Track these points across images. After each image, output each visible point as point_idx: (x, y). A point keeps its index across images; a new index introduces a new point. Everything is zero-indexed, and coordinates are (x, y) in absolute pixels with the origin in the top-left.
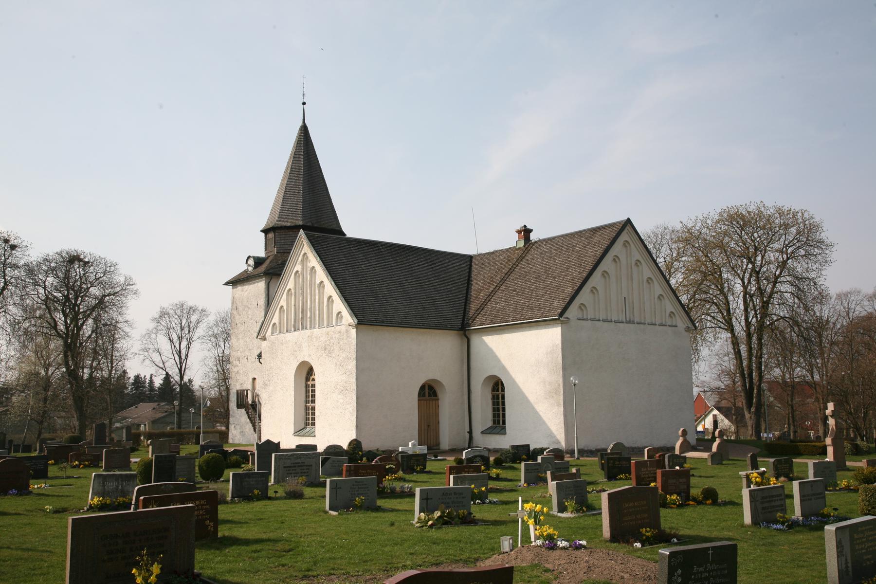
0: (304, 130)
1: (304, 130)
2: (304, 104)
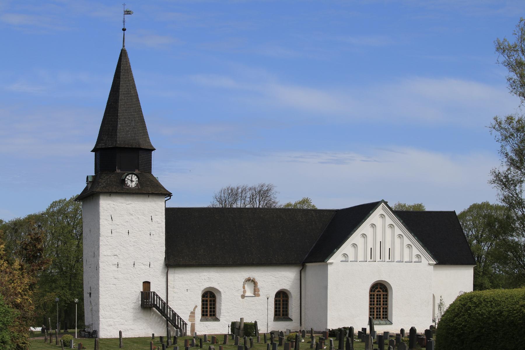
0: (123, 54)
1: (123, 54)
2: (124, 30)
